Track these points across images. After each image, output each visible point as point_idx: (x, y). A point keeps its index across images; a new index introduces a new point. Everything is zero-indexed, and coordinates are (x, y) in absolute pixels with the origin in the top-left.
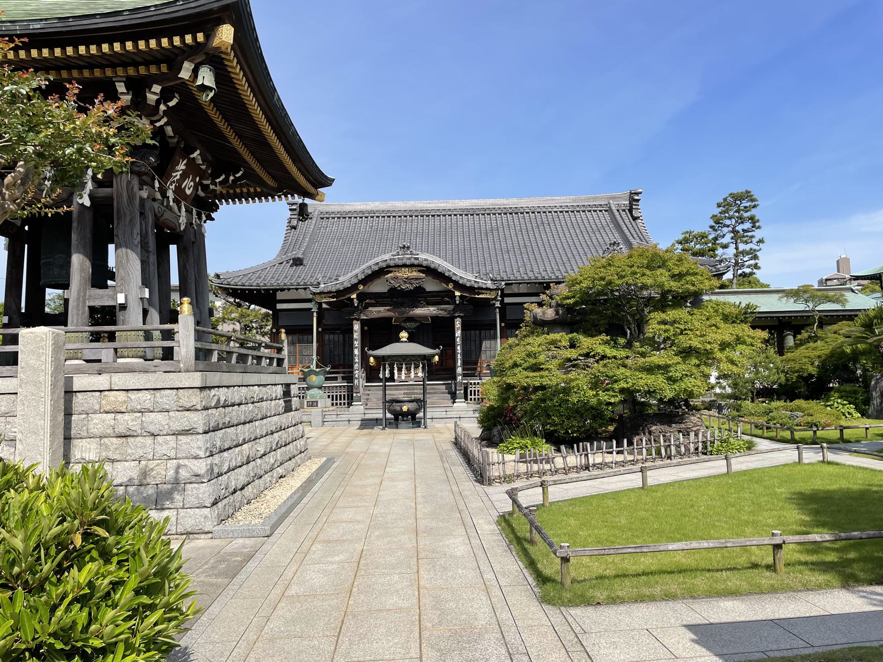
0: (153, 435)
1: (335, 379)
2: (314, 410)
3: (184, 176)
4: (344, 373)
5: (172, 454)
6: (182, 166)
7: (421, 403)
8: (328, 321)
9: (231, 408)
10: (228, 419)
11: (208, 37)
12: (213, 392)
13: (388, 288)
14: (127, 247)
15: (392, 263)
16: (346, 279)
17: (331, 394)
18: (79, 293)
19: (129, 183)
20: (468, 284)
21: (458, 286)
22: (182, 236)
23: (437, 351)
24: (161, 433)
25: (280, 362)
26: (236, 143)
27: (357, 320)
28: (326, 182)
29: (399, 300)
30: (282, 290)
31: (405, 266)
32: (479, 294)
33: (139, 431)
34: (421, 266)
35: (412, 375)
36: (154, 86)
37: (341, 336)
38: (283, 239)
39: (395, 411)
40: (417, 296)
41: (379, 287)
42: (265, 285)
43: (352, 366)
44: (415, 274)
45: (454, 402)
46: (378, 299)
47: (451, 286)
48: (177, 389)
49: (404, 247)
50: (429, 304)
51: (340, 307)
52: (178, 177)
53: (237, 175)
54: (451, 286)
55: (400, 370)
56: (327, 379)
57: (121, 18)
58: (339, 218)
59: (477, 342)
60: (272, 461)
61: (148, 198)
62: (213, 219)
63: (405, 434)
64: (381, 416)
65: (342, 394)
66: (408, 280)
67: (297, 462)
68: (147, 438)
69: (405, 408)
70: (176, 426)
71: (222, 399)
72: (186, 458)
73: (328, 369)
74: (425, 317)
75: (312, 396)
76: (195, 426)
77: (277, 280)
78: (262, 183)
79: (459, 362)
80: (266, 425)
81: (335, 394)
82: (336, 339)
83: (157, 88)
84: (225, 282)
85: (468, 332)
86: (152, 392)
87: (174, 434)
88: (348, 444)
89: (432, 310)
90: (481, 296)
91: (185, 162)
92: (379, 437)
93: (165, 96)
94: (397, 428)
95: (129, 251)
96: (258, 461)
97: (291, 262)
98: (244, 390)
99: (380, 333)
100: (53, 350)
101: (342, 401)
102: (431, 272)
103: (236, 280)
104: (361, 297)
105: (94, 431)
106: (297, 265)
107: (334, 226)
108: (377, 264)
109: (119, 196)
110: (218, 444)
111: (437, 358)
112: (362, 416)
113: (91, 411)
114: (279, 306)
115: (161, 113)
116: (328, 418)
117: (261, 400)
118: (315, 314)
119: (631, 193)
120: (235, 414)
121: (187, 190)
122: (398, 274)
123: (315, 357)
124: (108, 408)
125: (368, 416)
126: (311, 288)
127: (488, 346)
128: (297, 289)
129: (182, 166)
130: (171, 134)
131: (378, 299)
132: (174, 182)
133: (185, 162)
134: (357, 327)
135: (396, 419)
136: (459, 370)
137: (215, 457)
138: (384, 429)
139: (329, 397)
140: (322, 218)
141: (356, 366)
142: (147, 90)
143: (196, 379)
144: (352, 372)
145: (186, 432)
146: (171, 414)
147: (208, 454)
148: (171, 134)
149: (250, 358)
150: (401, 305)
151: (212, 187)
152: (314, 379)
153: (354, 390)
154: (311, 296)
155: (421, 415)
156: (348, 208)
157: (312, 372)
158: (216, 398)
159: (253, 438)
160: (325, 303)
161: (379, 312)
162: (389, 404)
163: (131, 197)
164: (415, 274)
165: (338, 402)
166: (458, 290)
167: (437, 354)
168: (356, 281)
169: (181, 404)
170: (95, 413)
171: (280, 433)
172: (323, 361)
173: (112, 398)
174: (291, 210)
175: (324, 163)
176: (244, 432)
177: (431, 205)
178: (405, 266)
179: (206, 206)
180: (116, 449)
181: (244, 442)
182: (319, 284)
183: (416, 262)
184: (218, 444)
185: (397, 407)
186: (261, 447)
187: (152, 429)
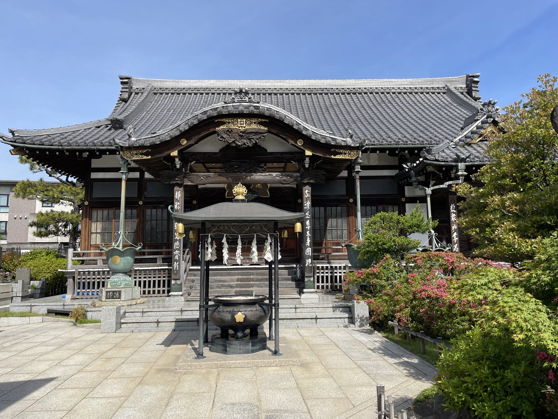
1: (154, 261)
7: (268, 306)
15: (225, 112)
16: (165, 132)
20: (323, 141)
21: (311, 142)
27: (180, 185)
32: (336, 154)
35: (255, 256)
39: (222, 321)
41: (210, 146)
45: (301, 292)
47: (300, 143)
54: (300, 143)
55: (232, 251)
56: (137, 261)
59: (322, 220)
65: (162, 279)
66: (245, 134)
69: (240, 317)
75: (115, 284)
79: (308, 241)
81: (152, 279)
85: (317, 209)
90: (338, 157)
94: (225, 351)
101: (161, 289)
104: (185, 156)
106: (116, 129)
108: (205, 112)
114: (94, 175)
116: (129, 318)
119: (468, 76)
122: (232, 127)
127: (334, 224)
131: (206, 160)
135: (225, 335)
136: (309, 251)
140: (155, 94)
141: (176, 245)
152: (121, 262)
153: (173, 276)
160: (134, 161)
162: (211, 306)
165: (156, 289)
166: (310, 149)
168: (178, 133)
172: (139, 235)
174: (122, 83)
183: (256, 111)
185: (225, 314)
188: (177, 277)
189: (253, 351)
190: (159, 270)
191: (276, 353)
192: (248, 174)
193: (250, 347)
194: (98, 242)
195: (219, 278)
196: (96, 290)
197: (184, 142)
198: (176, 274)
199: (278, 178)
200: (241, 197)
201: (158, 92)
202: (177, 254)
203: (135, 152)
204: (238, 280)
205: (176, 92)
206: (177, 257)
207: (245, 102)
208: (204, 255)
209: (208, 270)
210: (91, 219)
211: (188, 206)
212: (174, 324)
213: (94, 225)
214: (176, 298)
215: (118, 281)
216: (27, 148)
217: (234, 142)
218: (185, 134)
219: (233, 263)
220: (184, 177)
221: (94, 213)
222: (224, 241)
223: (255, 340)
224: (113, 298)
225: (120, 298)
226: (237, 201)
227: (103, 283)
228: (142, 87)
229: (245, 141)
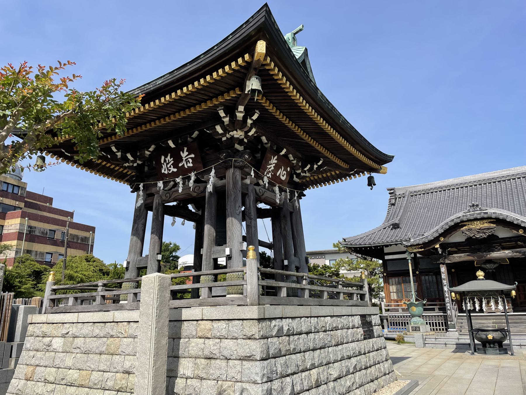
0: (226, 359)
1: (433, 310)
2: (416, 334)
3: (277, 167)
4: (440, 305)
5: (238, 377)
6: (274, 161)
8: (423, 265)
9: (296, 337)
10: (292, 346)
11: (252, 56)
12: (274, 323)
13: (466, 238)
14: (232, 217)
15: (465, 219)
16: (430, 234)
17: (428, 321)
18: (207, 250)
19: (234, 173)
22: (282, 208)
23: (514, 286)
24: (232, 358)
25: (362, 297)
26: (306, 137)
27: (443, 264)
28: (388, 159)
29: (476, 247)
30: (387, 246)
31: (476, 219)
33: (218, 355)
34: (491, 218)
36: (240, 107)
37: (434, 277)
38: (387, 212)
40: (491, 242)
41: (457, 238)
42: (374, 243)
43: (444, 300)
44: (486, 225)
46: (459, 247)
48: (243, 320)
49: (473, 205)
50: (504, 248)
51: (428, 256)
52: (272, 168)
53: (319, 164)
56: (425, 310)
57: (200, 61)
58: (423, 194)
60: (348, 384)
61: (251, 183)
62: (304, 195)
63: (492, 360)
64: (468, 341)
65: (440, 321)
67: (379, 384)
68: (223, 361)
69: (490, 337)
70: (242, 353)
71: (285, 328)
72: (248, 382)
73: (425, 302)
74: (503, 259)
75: (415, 323)
76: (254, 353)
77: (382, 239)
78: (338, 167)
80: (340, 350)
81: (434, 321)
82: (431, 279)
83: (241, 108)
84: (349, 244)
86: (227, 322)
87: (240, 359)
88: (438, 367)
89: (507, 253)
91: (276, 157)
92: (469, 361)
93: (249, 113)
94: (485, 353)
95: (233, 219)
96: (331, 384)
97: (392, 227)
98: (314, 320)
99: (462, 273)
100: (159, 289)
102: (500, 222)
103: (356, 242)
105: (193, 353)
106: (395, 228)
107: (420, 200)
108: (453, 220)
109: (229, 183)
110: (279, 370)
111: (514, 293)
112: (457, 341)
113: (191, 336)
114: (387, 257)
115: (249, 125)
117: (336, 329)
118: (410, 261)
120: (301, 342)
121: (281, 177)
123: (413, 293)
124: (200, 334)
125: (462, 341)
126: (404, 243)
128: (396, 245)
129: (274, 161)
130: (266, 141)
131: (459, 247)
132: (270, 172)
133: (276, 157)
134: (443, 269)
137: (274, 382)
138: (473, 354)
139: (427, 323)
142: (236, 111)
143: (253, 312)
144: (445, 305)
145: (248, 358)
146: (239, 341)
147: (265, 380)
148: (266, 141)
149: (355, 295)
150: (479, 250)
151: (302, 174)
154: (404, 249)
155: (506, 342)
156: (429, 187)
157: (411, 305)
158: (276, 328)
159: (325, 362)
161: (461, 257)
162: (474, 332)
163: (235, 183)
164: (486, 225)
165: (438, 327)
167: (514, 289)
169: (244, 333)
170: (193, 338)
171: (359, 358)
172: (420, 295)
173: (203, 326)
174: (390, 193)
175: (382, 146)
176: (310, 358)
177: (496, 174)
178: (476, 219)
179: (299, 188)
180: (203, 369)
181: (313, 367)
182: (410, 239)
183: (486, 216)
184: (279, 370)
185: (483, 335)
186: (334, 371)
187: (226, 353)
188: (451, 320)
189: (500, 354)
190: (438, 316)
191: (512, 354)
192: (488, 253)
193: (498, 351)
194: (396, 298)
195: (479, 321)
196: (404, 327)
197: (442, 239)
198: (450, 318)
199: (510, 254)
200: (481, 277)
201: (414, 194)
202: (448, 306)
203: (414, 247)
204: (493, 323)
205: (426, 192)
206: (449, 308)
207: (477, 211)
208: (466, 307)
209: (470, 316)
210: (389, 284)
211: (455, 281)
212: (455, 346)
213: (391, 287)
214: (453, 333)
215: (416, 321)
216: (353, 247)
217: (474, 236)
218: (441, 235)
219: (489, 311)
220: (445, 258)
221: (390, 281)
222: (476, 300)
223: (501, 349)
224: (416, 330)
225: (419, 331)
226: (480, 279)
227: (408, 323)
228: (401, 193)
229: (481, 235)
